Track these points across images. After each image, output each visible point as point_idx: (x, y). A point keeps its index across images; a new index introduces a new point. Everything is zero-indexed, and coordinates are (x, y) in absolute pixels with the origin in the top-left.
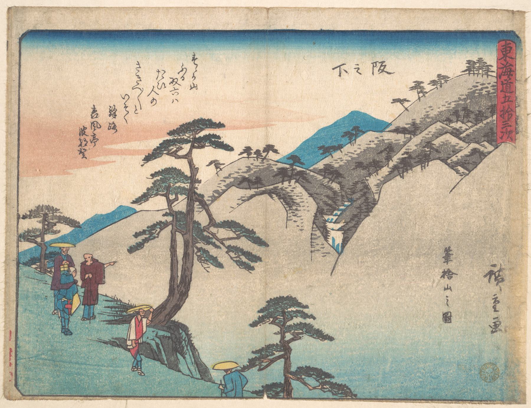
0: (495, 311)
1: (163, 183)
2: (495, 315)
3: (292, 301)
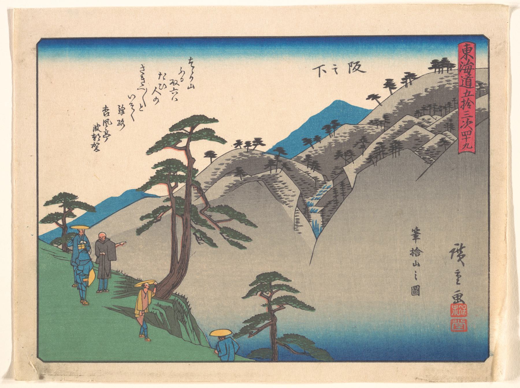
0: (457, 284)
1: (166, 172)
2: (458, 287)
3: (276, 275)
